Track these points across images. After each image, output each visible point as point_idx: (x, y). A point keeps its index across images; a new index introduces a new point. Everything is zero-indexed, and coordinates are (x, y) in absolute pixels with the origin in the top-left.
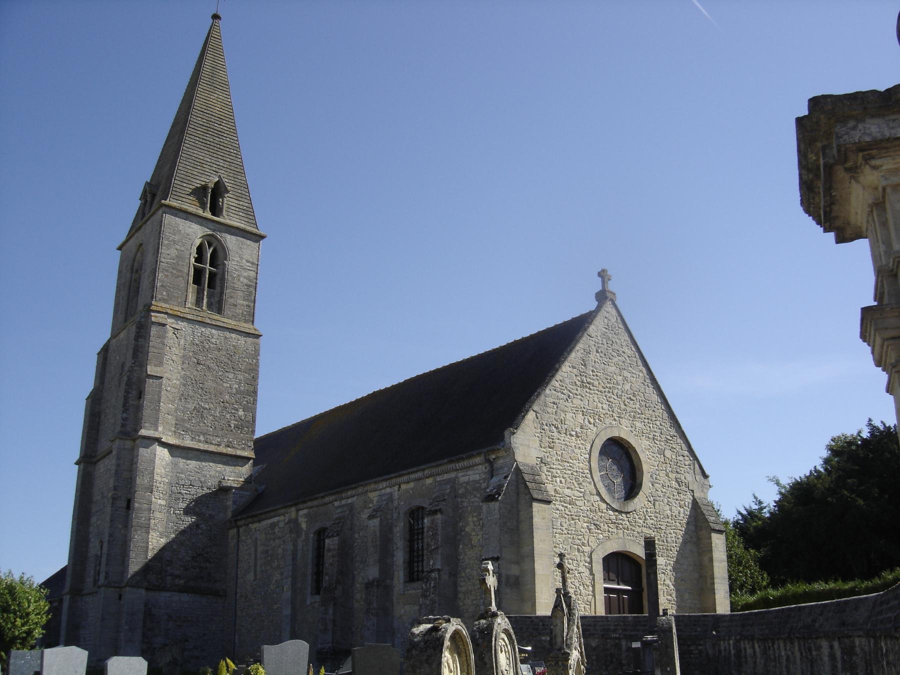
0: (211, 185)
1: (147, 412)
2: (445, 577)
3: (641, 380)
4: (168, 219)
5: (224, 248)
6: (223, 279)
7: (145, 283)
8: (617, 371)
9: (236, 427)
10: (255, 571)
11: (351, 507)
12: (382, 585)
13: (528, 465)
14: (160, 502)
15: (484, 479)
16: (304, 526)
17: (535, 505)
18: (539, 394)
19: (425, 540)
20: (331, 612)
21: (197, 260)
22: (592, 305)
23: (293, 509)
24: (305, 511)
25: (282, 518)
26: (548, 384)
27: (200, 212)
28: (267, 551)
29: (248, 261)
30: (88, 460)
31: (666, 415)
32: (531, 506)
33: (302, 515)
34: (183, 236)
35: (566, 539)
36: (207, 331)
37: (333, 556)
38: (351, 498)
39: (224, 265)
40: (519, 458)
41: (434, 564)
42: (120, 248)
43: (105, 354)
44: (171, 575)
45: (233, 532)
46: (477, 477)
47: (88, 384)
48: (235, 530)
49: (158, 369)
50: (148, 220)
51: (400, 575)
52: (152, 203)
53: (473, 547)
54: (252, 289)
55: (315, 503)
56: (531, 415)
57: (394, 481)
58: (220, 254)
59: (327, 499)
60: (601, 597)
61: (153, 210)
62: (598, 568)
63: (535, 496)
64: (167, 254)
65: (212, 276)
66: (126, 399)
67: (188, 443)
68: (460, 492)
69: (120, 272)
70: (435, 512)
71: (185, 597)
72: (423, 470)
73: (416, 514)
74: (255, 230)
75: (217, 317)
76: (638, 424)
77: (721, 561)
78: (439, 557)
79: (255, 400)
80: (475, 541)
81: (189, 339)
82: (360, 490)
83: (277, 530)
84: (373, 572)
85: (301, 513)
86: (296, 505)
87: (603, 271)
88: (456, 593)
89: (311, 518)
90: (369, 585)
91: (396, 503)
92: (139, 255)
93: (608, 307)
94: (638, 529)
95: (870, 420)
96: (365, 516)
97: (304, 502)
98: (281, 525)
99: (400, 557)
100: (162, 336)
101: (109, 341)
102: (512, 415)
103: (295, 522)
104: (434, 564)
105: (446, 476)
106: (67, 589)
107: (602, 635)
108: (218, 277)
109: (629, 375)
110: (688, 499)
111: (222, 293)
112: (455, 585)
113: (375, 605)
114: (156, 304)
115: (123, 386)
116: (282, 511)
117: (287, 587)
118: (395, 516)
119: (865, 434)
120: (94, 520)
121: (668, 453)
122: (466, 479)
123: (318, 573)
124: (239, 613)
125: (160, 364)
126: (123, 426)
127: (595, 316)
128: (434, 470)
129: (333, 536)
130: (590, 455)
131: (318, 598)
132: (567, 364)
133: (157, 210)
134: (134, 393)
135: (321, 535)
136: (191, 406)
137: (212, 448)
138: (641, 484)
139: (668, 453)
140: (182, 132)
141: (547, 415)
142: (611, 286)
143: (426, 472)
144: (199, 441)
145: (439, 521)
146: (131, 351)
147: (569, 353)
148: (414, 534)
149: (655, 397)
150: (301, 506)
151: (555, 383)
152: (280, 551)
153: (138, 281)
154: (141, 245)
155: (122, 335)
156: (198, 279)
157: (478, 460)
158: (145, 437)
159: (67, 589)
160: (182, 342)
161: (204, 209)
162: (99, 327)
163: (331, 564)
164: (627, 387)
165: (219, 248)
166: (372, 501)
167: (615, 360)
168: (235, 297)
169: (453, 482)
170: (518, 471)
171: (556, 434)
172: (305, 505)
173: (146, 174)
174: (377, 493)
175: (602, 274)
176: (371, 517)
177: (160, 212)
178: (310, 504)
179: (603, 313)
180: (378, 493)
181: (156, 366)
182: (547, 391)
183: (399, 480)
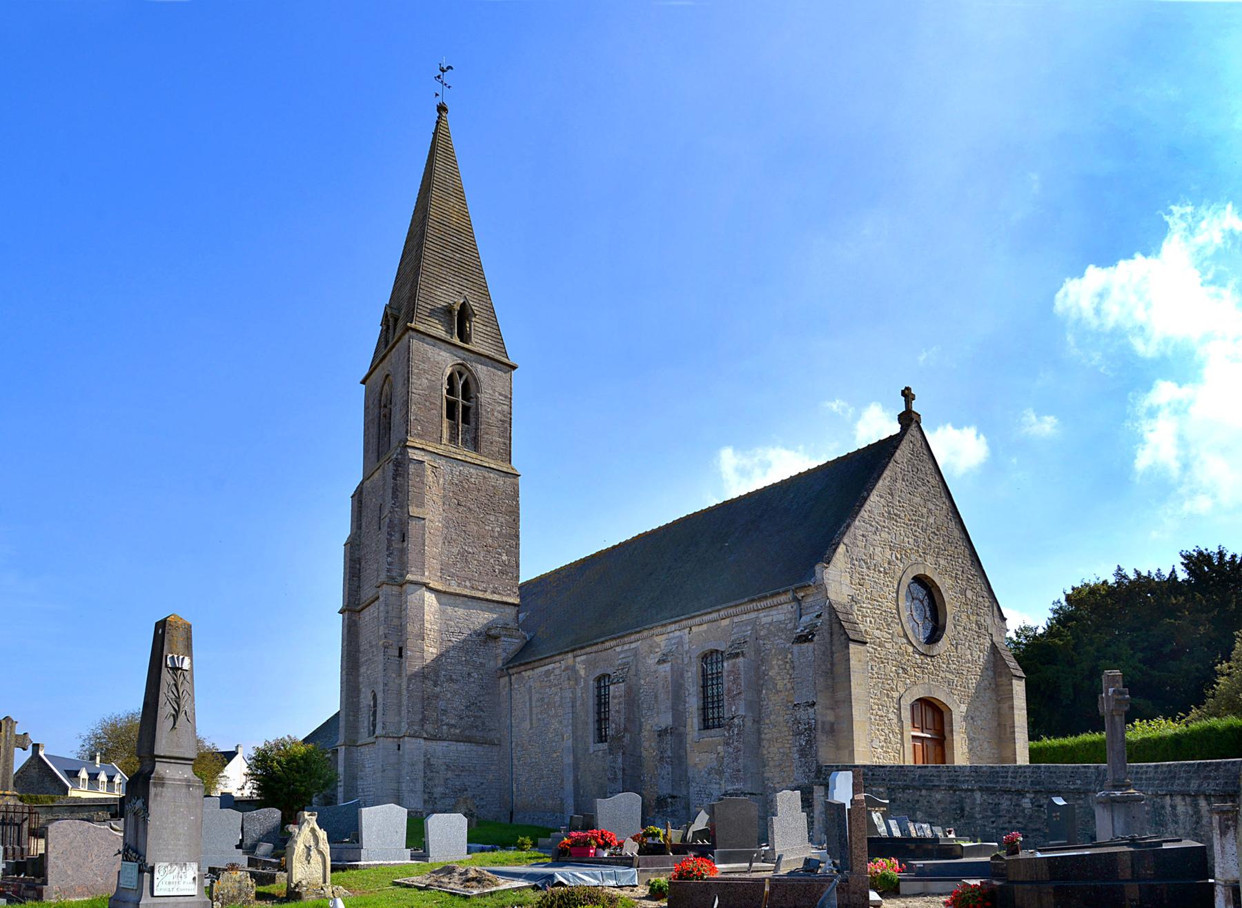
0: (457, 307)
1: (412, 556)
2: (749, 723)
3: (944, 512)
4: (416, 344)
5: (475, 379)
6: (477, 413)
7: (397, 418)
8: (922, 503)
9: (501, 572)
10: (531, 720)
11: (636, 652)
12: (673, 733)
13: (839, 603)
14: (431, 650)
15: (791, 619)
16: (582, 673)
17: (852, 646)
18: (849, 526)
19: (726, 686)
20: (620, 760)
21: (449, 392)
22: (896, 428)
23: (570, 655)
24: (583, 658)
25: (558, 665)
26: (857, 513)
27: (448, 337)
28: (543, 699)
29: (500, 394)
30: (352, 609)
31: (967, 552)
32: (848, 647)
33: (580, 662)
34: (433, 363)
35: (876, 684)
36: (466, 470)
37: (620, 703)
38: (635, 643)
39: (477, 398)
40: (832, 596)
41: (737, 710)
42: (363, 382)
43: (359, 497)
44: (447, 724)
45: (504, 680)
46: (782, 617)
47: (345, 531)
48: (507, 678)
49: (421, 510)
50: (393, 346)
51: (693, 721)
52: (395, 325)
53: (778, 692)
54: (507, 425)
55: (595, 648)
56: (841, 549)
57: (684, 623)
58: (473, 386)
59: (607, 645)
60: (909, 745)
61: (398, 334)
62: (906, 714)
63: (851, 637)
64: (419, 384)
65: (466, 409)
66: (389, 541)
67: (454, 588)
68: (762, 633)
69: (366, 408)
70: (737, 655)
71: (462, 747)
72: (719, 610)
73: (710, 657)
74: (506, 360)
75: (474, 455)
76: (942, 562)
77: (1021, 709)
78: (742, 702)
79: (518, 545)
80: (780, 686)
81: (448, 478)
82: (645, 633)
83: (552, 677)
84: (666, 720)
85: (578, 659)
86: (573, 651)
87: (908, 389)
88: (760, 740)
89: (590, 665)
90: (662, 733)
91: (686, 647)
92: (386, 387)
93: (913, 429)
94: (942, 674)
95: (1119, 569)
96: (652, 660)
97: (583, 648)
98: (557, 672)
99: (693, 703)
100: (421, 475)
101: (362, 483)
102: (823, 550)
103: (573, 669)
104: (737, 710)
105: (745, 617)
106: (341, 740)
107: (951, 788)
108: (472, 411)
109: (933, 507)
110: (988, 644)
111: (477, 429)
112: (759, 732)
113: (669, 753)
114: (413, 441)
115: (385, 529)
116: (558, 658)
117: (568, 735)
118: (686, 660)
119: (1112, 580)
120: (363, 670)
121: (969, 594)
122: (769, 619)
123: (602, 719)
124: (515, 761)
125: (421, 505)
126: (388, 571)
127: (901, 441)
128: (731, 611)
129: (618, 682)
130: (897, 593)
131: (604, 746)
132: (875, 492)
133: (403, 334)
134: (397, 536)
135: (602, 682)
136: (455, 550)
137: (480, 595)
138: (944, 627)
139: (969, 594)
140: (420, 245)
141: (857, 550)
142: (915, 407)
143: (722, 613)
144: (466, 587)
145: (741, 665)
146: (390, 491)
147: (877, 481)
148: (708, 680)
149: (957, 533)
150: (579, 652)
151: (864, 514)
152: (557, 698)
153: (388, 417)
154: (387, 376)
155: (376, 475)
156: (451, 414)
157: (782, 598)
158: (412, 582)
159: (341, 740)
160: (441, 481)
161: (452, 335)
162: (348, 467)
163: (618, 712)
164: (931, 520)
165: (471, 380)
166: (658, 646)
167: (920, 489)
168: (489, 435)
169: (754, 623)
170: (832, 610)
171: (865, 570)
172: (583, 651)
173: (384, 295)
174: (663, 638)
175: (907, 394)
176: (661, 661)
177: (406, 336)
178: (588, 650)
179: (908, 437)
180: (665, 636)
181: (417, 506)
182: (857, 522)
183: (690, 622)
